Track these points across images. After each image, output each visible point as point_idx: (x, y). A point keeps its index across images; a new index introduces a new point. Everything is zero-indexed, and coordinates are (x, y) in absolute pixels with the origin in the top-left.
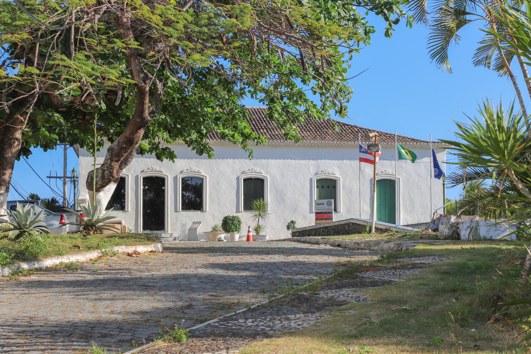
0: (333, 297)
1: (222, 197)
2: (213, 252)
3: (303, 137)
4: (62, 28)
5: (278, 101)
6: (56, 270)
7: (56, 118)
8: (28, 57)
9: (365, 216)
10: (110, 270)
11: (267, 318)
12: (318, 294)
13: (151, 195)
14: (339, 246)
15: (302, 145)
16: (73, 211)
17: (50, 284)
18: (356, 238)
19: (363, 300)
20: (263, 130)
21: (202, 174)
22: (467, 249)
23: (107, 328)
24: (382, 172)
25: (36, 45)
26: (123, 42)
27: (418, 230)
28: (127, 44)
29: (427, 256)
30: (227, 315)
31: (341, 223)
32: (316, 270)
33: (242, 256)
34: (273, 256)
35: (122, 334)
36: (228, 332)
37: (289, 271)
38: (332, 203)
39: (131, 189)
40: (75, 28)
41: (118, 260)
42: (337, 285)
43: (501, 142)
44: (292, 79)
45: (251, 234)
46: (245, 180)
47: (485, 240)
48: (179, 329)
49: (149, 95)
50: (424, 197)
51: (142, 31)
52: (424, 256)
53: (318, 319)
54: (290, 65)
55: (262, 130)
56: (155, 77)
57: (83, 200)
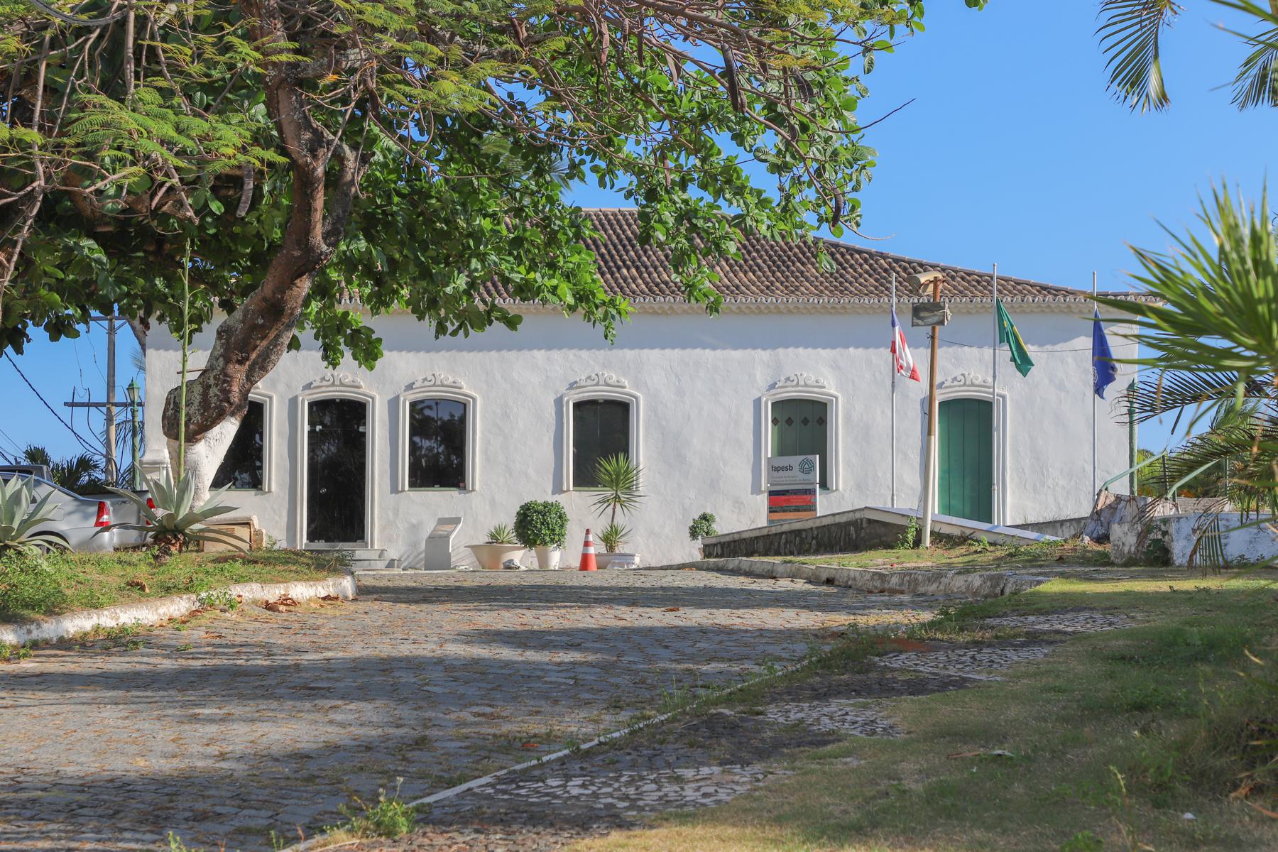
0: (801, 721)
1: (518, 451)
2: (487, 600)
3: (737, 287)
4: (102, 21)
5: (666, 197)
6: (83, 645)
7: (86, 251)
8: (19, 97)
9: (905, 503)
10: (220, 646)
11: (621, 776)
12: (759, 713)
13: (330, 448)
14: (830, 582)
15: (734, 308)
16: (128, 492)
17: (69, 682)
18: (877, 560)
19: (884, 729)
20: (628, 269)
21: (465, 390)
22: (1187, 592)
23: (208, 797)
24: (955, 379)
25: (38, 68)
26: (257, 49)
27: (1054, 538)
28: (265, 54)
29: (1072, 610)
30: (518, 767)
31: (838, 519)
32: (761, 648)
33: (563, 611)
34: (648, 610)
35: (245, 812)
36: (518, 812)
37: (689, 651)
38: (814, 467)
39: (280, 433)
40: (137, 17)
41: (240, 619)
42: (814, 689)
43: (1260, 301)
44: (706, 132)
45: (592, 550)
46: (577, 406)
47: (1243, 566)
48: (390, 801)
49: (326, 187)
50: (1071, 448)
51: (308, 21)
52: (1065, 610)
53: (758, 780)
54: (703, 97)
55: (624, 271)
56: (341, 139)
57: (155, 463)
